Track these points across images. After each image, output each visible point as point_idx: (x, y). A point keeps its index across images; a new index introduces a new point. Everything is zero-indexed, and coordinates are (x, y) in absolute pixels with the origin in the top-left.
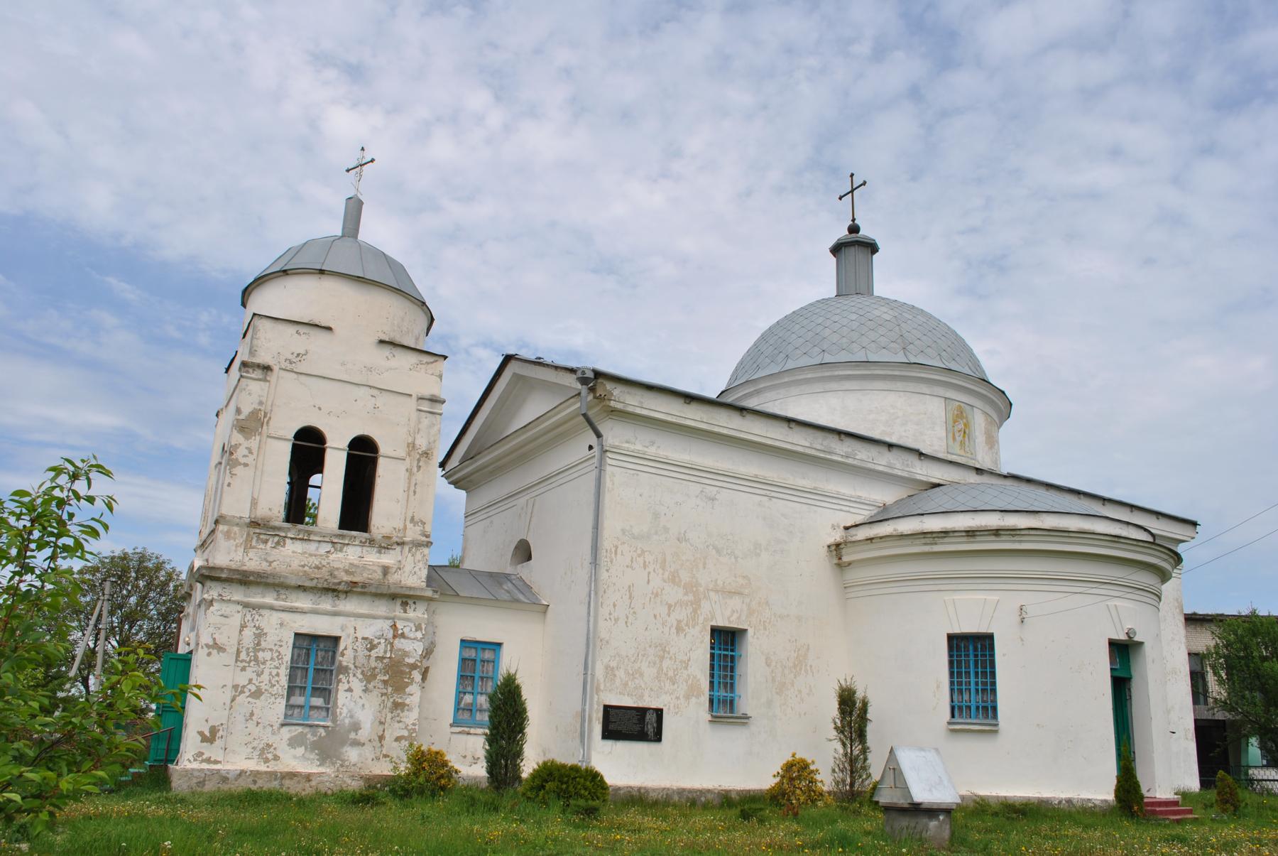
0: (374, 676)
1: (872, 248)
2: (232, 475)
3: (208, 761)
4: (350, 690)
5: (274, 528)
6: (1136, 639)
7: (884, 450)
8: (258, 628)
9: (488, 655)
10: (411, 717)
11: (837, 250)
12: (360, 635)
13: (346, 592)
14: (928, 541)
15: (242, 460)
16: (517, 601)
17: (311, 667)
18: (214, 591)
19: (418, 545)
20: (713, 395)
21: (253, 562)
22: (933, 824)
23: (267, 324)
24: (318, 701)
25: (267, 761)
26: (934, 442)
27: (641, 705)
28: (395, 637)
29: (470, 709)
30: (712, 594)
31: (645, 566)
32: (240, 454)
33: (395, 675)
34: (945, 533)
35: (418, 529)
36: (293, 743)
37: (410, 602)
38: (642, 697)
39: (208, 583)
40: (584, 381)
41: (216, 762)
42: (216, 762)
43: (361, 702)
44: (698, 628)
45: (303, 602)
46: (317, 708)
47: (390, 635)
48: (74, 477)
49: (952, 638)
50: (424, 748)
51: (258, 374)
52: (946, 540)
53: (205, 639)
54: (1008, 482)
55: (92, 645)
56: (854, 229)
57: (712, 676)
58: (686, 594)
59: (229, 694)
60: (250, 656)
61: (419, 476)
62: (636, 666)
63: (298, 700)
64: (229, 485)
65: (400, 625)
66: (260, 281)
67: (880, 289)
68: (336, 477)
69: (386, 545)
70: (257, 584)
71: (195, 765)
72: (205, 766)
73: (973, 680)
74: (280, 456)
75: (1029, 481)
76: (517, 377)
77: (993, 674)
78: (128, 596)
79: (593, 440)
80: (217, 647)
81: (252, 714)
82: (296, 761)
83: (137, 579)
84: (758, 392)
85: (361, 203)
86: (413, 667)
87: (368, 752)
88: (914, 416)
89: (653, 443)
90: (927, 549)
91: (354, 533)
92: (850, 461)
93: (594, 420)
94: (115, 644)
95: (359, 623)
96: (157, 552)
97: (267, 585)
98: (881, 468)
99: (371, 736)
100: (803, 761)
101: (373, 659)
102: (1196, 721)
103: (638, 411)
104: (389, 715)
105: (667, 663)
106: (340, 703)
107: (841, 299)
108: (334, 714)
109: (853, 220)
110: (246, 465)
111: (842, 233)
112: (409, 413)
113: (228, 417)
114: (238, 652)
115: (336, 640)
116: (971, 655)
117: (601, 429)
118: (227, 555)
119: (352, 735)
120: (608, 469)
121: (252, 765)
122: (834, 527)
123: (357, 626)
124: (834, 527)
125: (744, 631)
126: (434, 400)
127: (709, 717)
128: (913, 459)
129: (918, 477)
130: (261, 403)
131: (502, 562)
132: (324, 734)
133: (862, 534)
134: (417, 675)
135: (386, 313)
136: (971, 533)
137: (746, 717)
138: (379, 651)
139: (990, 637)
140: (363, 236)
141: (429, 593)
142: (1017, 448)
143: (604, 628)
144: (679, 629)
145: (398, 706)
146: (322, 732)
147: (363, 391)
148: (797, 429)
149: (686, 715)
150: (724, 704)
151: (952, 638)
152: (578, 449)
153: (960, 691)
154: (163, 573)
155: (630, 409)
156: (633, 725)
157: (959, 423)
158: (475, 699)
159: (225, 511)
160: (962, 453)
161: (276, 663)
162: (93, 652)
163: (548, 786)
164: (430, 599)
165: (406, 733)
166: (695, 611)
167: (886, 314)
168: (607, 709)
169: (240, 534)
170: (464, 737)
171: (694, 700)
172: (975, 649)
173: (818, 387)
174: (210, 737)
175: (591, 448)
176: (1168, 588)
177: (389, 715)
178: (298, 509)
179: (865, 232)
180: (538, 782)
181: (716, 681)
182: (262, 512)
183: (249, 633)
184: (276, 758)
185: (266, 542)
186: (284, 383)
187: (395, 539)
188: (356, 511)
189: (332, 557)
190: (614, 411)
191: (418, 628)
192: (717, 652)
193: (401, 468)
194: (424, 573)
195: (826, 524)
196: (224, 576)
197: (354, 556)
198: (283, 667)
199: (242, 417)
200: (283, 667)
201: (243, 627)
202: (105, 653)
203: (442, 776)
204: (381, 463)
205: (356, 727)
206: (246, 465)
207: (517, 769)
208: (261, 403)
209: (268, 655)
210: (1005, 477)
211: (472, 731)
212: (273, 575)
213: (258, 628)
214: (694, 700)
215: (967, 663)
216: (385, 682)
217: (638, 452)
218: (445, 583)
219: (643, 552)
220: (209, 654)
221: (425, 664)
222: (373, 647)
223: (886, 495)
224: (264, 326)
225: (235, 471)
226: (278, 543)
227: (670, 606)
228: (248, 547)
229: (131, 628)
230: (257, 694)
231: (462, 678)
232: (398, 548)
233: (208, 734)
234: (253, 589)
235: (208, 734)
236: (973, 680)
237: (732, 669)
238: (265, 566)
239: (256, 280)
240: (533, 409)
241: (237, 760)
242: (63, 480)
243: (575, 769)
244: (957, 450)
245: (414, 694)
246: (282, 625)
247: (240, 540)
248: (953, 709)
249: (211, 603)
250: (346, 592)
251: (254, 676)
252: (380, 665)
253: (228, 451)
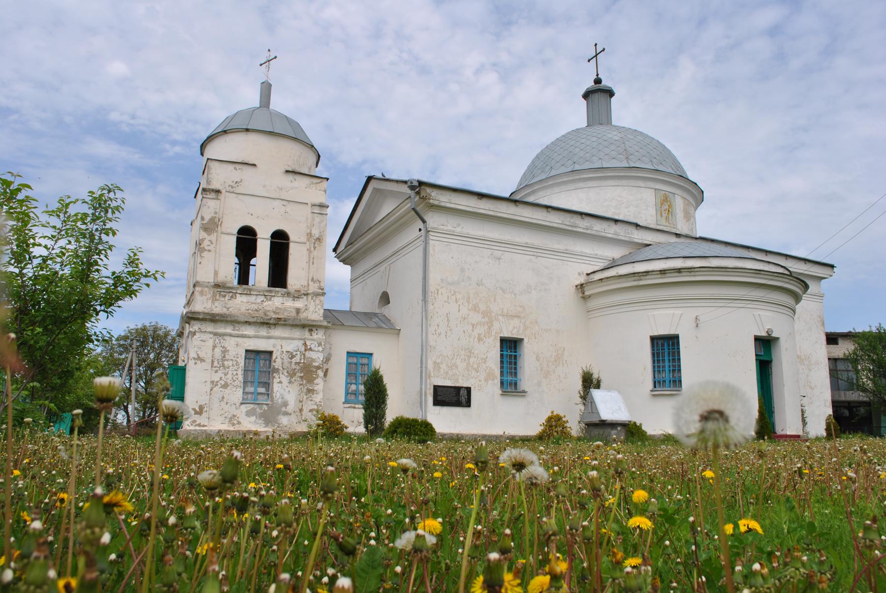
0: (294, 374)
1: (610, 93)
2: (202, 257)
3: (199, 425)
4: (280, 382)
5: (229, 288)
6: (774, 335)
7: (612, 224)
9: (365, 361)
10: (318, 398)
11: (586, 96)
12: (284, 350)
13: (275, 325)
14: (636, 278)
15: (207, 248)
16: (381, 328)
17: (257, 369)
18: (196, 326)
19: (317, 295)
20: (507, 195)
21: (218, 308)
22: (614, 432)
23: (216, 164)
25: (233, 425)
26: (648, 217)
27: (457, 385)
28: (306, 350)
29: (354, 393)
30: (500, 317)
31: (456, 301)
32: (205, 244)
33: (307, 373)
34: (647, 273)
35: (317, 285)
36: (249, 414)
37: (314, 329)
38: (458, 380)
39: (192, 322)
40: (412, 188)
41: (204, 426)
42: (204, 426)
43: (287, 389)
44: (492, 338)
45: (249, 331)
46: (261, 394)
47: (303, 349)
48: (109, 191)
49: (653, 339)
50: (326, 415)
51: (213, 195)
52: (648, 277)
53: (193, 355)
54: (699, 241)
55: (128, 385)
56: (598, 81)
57: (502, 367)
58: (483, 317)
59: (209, 386)
60: (220, 363)
61: (315, 253)
62: (454, 361)
63: (250, 389)
65: (308, 343)
66: (211, 138)
67: (615, 122)
68: (263, 254)
69: (297, 295)
70: (222, 321)
71: (192, 428)
72: (197, 428)
73: (667, 364)
74: (230, 244)
75: (713, 241)
76: (376, 190)
77: (679, 360)
78: (149, 353)
79: (421, 225)
80: (199, 359)
81: (223, 398)
82: (250, 424)
83: (153, 342)
84: (533, 192)
85: (270, 85)
86: (318, 368)
87: (293, 419)
88: (635, 202)
89: (459, 225)
90: (636, 283)
91: (277, 289)
92: (589, 232)
93: (421, 213)
94: (143, 384)
95: (284, 343)
96: (165, 325)
97: (227, 322)
98: (610, 236)
99: (295, 407)
100: (558, 415)
101: (293, 364)
103: (448, 205)
104: (305, 397)
105: (472, 360)
106: (275, 390)
108: (272, 396)
109: (597, 75)
110: (209, 251)
111: (590, 84)
112: (316, 222)
113: (198, 224)
114: (213, 362)
115: (271, 353)
116: (666, 348)
117: (426, 218)
118: (202, 305)
119: (284, 409)
120: (431, 242)
121: (225, 427)
122: (579, 274)
123: (282, 344)
124: (579, 274)
125: (522, 339)
126: (322, 206)
127: (500, 392)
129: (636, 241)
130: (216, 213)
133: (597, 277)
134: (321, 373)
135: (289, 154)
136: (663, 272)
137: (524, 392)
138: (297, 359)
139: (676, 337)
141: (325, 323)
142: (708, 221)
143: (432, 340)
144: (480, 339)
145: (310, 391)
146: (265, 407)
147: (277, 203)
148: (553, 212)
150: (510, 384)
151: (653, 339)
152: (413, 232)
153: (659, 372)
154: (170, 337)
155: (443, 204)
156: (453, 397)
157: (665, 205)
158: (358, 388)
159: (199, 279)
160: (667, 224)
161: (235, 368)
162: (129, 390)
163: (399, 430)
164: (326, 328)
165: (316, 407)
166: (489, 328)
167: (615, 136)
169: (209, 292)
170: (352, 410)
171: (490, 382)
172: (669, 345)
173: (571, 186)
174: (200, 411)
175: (420, 230)
176: (806, 305)
177: (305, 397)
178: (243, 278)
179: (606, 83)
180: (393, 429)
181: (505, 371)
182: (221, 278)
183: (218, 351)
184: (239, 423)
185: (225, 296)
186: (229, 201)
187: (303, 292)
188: (278, 276)
189: (265, 304)
190: (432, 206)
191: (320, 345)
192: (505, 353)
193: (304, 249)
195: (574, 272)
196: (201, 317)
197: (278, 303)
198: (240, 370)
199: (205, 222)
200: (240, 370)
201: (214, 347)
202: (136, 390)
203: (337, 429)
204: (292, 247)
205: (285, 404)
206: (209, 251)
207: (382, 424)
208: (216, 213)
209: (230, 363)
210: (696, 238)
211: (357, 406)
212: (230, 315)
214: (490, 382)
215: (663, 353)
216: (301, 377)
217: (450, 231)
218: (334, 320)
219: (455, 292)
220: (196, 363)
221: (325, 366)
222: (293, 357)
223: (616, 253)
224: (214, 167)
225: (203, 254)
226: (232, 297)
227: (473, 325)
228: (214, 300)
229: (152, 373)
230: (225, 386)
231: (349, 374)
232: (305, 297)
234: (219, 325)
236: (667, 364)
237: (515, 364)
238: (225, 311)
239: (208, 138)
240: (387, 208)
241: (216, 424)
242: (105, 192)
243: (415, 421)
244: (663, 222)
245: (319, 384)
246: (237, 345)
247: (209, 296)
248: (655, 382)
249: (194, 333)
250: (275, 325)
251: (223, 375)
252: (298, 367)
253: (199, 244)
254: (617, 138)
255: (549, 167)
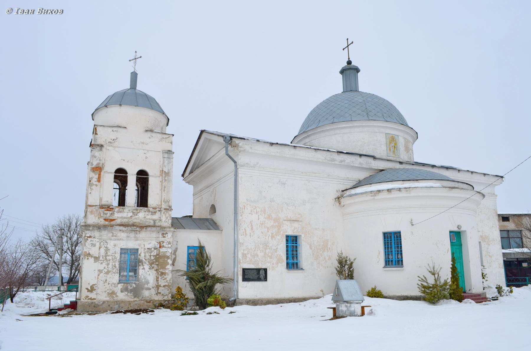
1: (357, 70)
4: (144, 269)
7: (358, 157)
8: (106, 247)
11: (342, 72)
24: (132, 274)
26: (381, 151)
27: (258, 267)
28: (160, 247)
31: (257, 213)
38: (258, 264)
51: (99, 148)
56: (349, 63)
59: (97, 273)
64: (90, 193)
69: (157, 210)
71: (86, 301)
81: (106, 280)
85: (136, 74)
87: (153, 292)
102: (504, 261)
105: (267, 251)
107: (348, 94)
109: (349, 59)
117: (235, 159)
122: (337, 191)
128: (371, 160)
129: (373, 168)
131: (206, 214)
132: (135, 286)
140: (139, 87)
143: (241, 238)
144: (273, 237)
149: (277, 271)
150: (293, 263)
156: (256, 275)
160: (394, 156)
165: (167, 284)
168: (244, 270)
171: (280, 264)
188: (143, 200)
194: (170, 221)
197: (143, 215)
205: (148, 283)
209: (110, 258)
213: (106, 247)
214: (280, 264)
215: (391, 243)
225: (92, 188)
230: (108, 272)
233: (89, 289)
235: (89, 289)
236: (393, 250)
244: (392, 154)
254: (361, 101)
255: (318, 120)
